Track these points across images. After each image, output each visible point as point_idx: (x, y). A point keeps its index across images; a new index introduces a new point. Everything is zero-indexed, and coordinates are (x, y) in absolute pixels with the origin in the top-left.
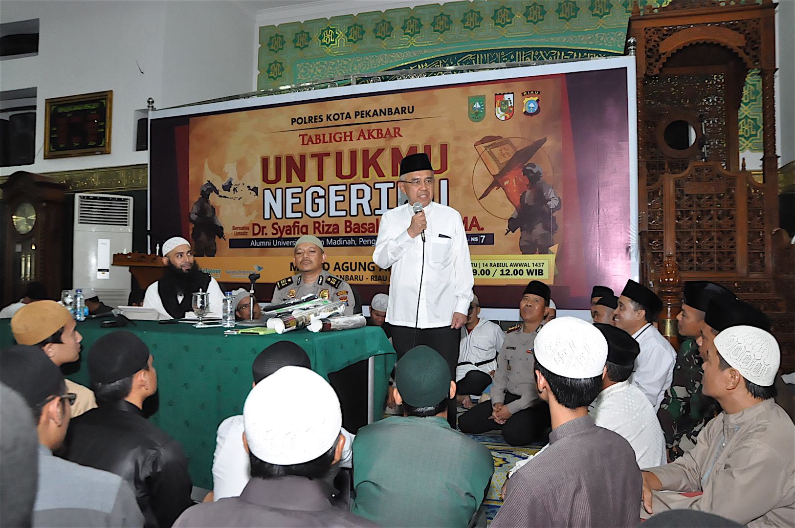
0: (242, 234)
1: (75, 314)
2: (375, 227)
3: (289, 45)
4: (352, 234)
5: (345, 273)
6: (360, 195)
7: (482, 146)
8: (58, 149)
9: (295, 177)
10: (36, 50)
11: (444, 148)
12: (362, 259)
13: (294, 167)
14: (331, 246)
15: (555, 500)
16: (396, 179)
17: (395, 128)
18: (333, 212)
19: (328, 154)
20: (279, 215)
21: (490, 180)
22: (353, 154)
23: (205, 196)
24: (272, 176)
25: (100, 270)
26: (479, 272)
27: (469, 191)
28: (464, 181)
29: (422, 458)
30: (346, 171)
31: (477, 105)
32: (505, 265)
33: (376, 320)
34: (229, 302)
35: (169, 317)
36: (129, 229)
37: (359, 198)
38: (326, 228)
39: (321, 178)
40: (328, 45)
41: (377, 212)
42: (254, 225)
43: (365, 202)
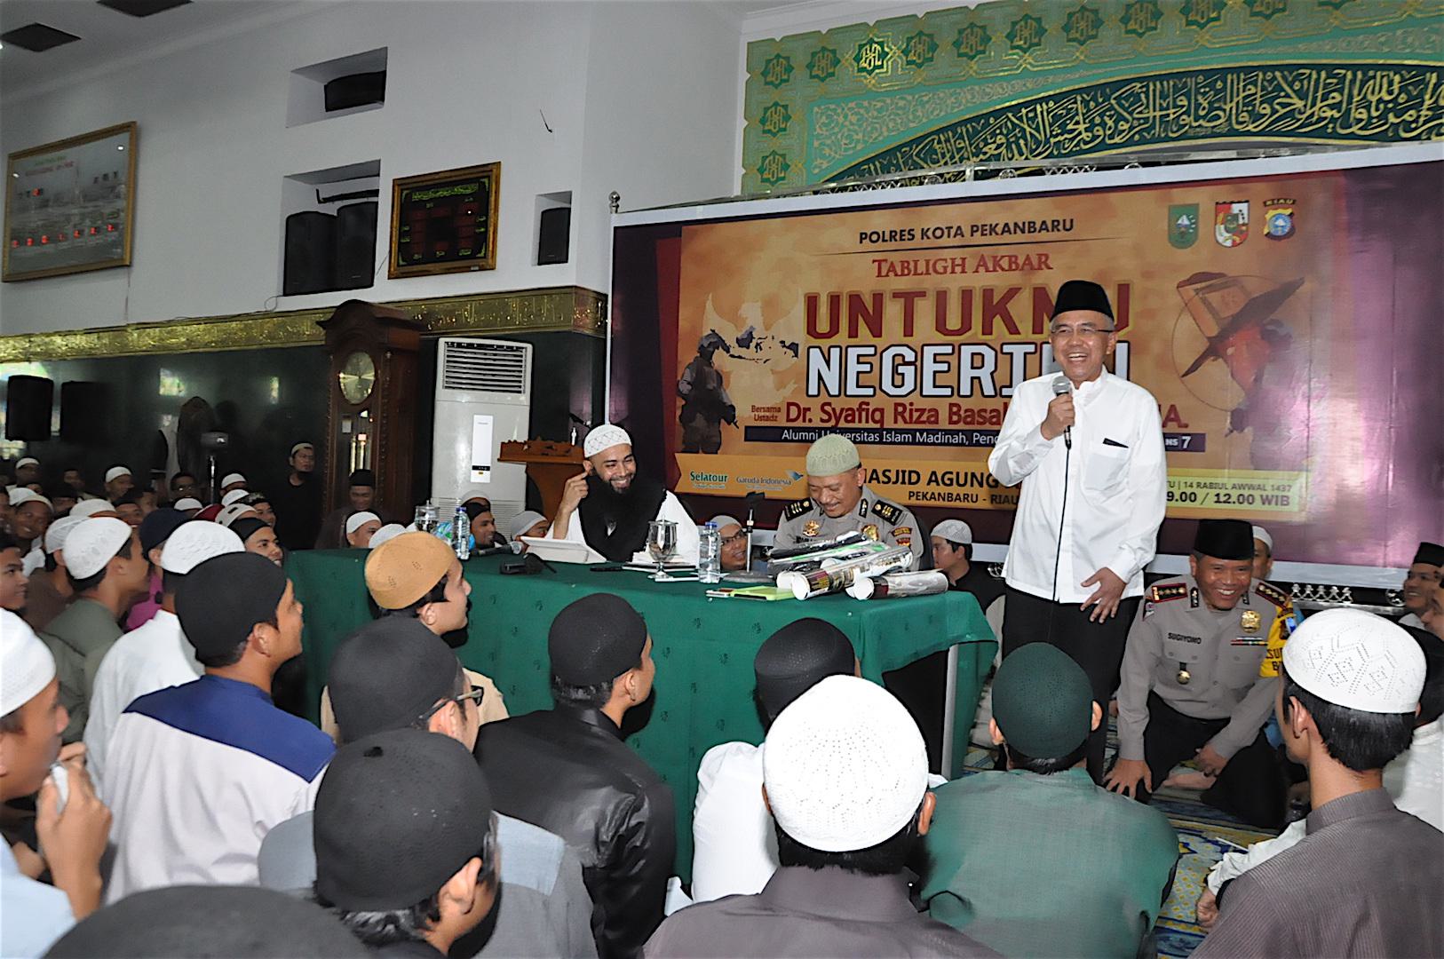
0: (767, 419)
1: (454, 547)
2: (999, 416)
3: (800, 74)
4: (961, 426)
5: (962, 491)
6: (977, 363)
7: (1190, 289)
8: (411, 262)
9: (863, 329)
10: (381, 98)
11: (1124, 290)
12: (974, 467)
13: (861, 313)
14: (924, 444)
15: (1317, 933)
16: (1038, 338)
17: (1040, 255)
18: (928, 389)
19: (922, 294)
20: (834, 390)
21: (1202, 346)
22: (967, 295)
23: (705, 354)
24: (823, 325)
25: (475, 468)
26: (1177, 496)
27: (1165, 362)
28: (1156, 347)
29: (1055, 844)
30: (953, 322)
31: (1184, 221)
32: (1224, 486)
33: (982, 582)
34: (711, 539)
35: (598, 558)
36: (525, 399)
37: (974, 368)
38: (916, 415)
39: (908, 332)
40: (870, 73)
41: (1005, 392)
42: (789, 404)
43: (984, 374)
